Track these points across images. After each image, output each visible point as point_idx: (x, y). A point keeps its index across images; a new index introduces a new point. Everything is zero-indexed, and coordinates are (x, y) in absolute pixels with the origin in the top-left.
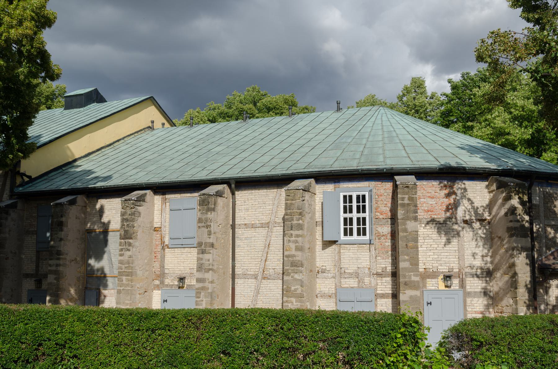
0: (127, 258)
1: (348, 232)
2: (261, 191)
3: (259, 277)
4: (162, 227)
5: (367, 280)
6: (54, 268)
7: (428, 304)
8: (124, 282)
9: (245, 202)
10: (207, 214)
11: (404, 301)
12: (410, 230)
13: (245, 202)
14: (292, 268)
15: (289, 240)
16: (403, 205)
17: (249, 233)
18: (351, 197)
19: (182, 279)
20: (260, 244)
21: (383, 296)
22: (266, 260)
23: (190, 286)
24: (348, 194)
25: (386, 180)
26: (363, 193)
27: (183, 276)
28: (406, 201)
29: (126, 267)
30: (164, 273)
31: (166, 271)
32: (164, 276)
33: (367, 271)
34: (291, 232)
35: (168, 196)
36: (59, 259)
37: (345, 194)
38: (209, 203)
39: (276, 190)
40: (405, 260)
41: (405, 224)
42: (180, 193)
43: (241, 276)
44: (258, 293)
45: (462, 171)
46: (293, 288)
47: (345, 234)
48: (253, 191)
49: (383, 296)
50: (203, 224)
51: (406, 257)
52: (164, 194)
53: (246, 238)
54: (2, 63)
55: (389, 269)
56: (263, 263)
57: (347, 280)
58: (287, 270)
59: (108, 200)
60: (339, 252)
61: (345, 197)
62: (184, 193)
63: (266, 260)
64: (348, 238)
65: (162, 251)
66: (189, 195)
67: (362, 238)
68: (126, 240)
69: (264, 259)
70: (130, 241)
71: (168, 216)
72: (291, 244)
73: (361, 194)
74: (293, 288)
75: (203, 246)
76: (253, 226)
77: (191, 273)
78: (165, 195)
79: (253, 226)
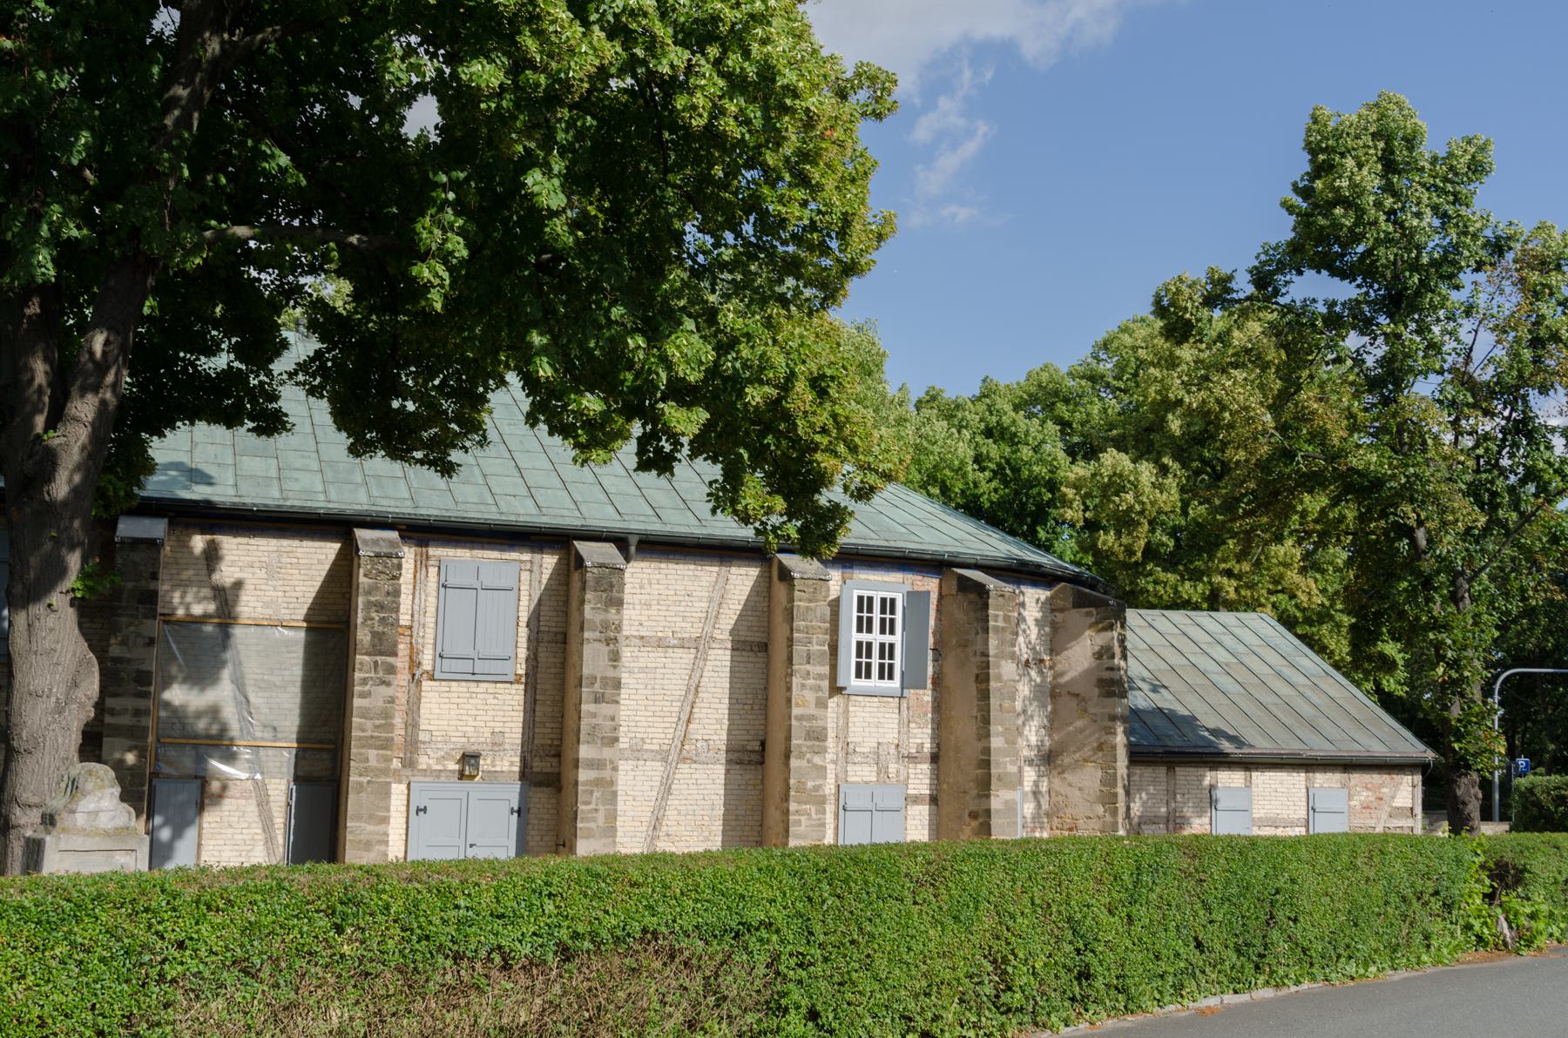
0: (381, 704)
1: (863, 671)
2: (681, 566)
3: (673, 757)
4: (416, 626)
5: (893, 768)
6: (126, 720)
7: (418, 810)
8: (373, 763)
9: (641, 587)
10: (607, 611)
11: (998, 811)
12: (1005, 678)
13: (641, 587)
14: (809, 743)
15: (803, 685)
16: (997, 629)
17: (652, 657)
18: (870, 599)
19: (469, 759)
20: (676, 683)
21: (916, 800)
22: (689, 721)
23: (493, 776)
24: (866, 594)
25: (747, 558)
26: (892, 595)
27: (473, 749)
28: (1001, 624)
29: (377, 727)
30: (417, 742)
31: (422, 736)
32: (417, 749)
33: (893, 750)
34: (808, 667)
35: (432, 551)
36: (146, 695)
37: (861, 593)
38: (612, 586)
39: (716, 569)
40: (998, 735)
41: (998, 666)
42: (472, 548)
43: (628, 754)
44: (669, 791)
45: (1033, 569)
46: (810, 784)
47: (858, 675)
48: (663, 565)
49: (916, 800)
50: (597, 635)
51: (1000, 729)
52: (423, 543)
53: (642, 670)
54: (8, 44)
55: (927, 747)
56: (682, 727)
57: (858, 768)
58: (799, 746)
59: (239, 540)
60: (847, 711)
61: (860, 599)
62: (483, 548)
63: (689, 721)
64: (863, 682)
65: (413, 686)
66: (495, 554)
67: (886, 683)
68: (379, 659)
69: (684, 717)
70: (390, 659)
71: (432, 600)
72: (806, 693)
73: (889, 595)
74: (810, 784)
75: (597, 685)
76: (661, 644)
77: (494, 744)
78: (427, 546)
79: (661, 644)
